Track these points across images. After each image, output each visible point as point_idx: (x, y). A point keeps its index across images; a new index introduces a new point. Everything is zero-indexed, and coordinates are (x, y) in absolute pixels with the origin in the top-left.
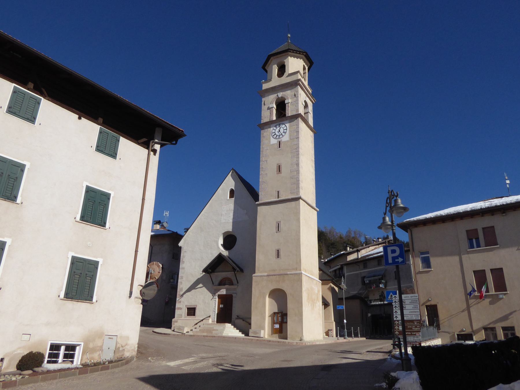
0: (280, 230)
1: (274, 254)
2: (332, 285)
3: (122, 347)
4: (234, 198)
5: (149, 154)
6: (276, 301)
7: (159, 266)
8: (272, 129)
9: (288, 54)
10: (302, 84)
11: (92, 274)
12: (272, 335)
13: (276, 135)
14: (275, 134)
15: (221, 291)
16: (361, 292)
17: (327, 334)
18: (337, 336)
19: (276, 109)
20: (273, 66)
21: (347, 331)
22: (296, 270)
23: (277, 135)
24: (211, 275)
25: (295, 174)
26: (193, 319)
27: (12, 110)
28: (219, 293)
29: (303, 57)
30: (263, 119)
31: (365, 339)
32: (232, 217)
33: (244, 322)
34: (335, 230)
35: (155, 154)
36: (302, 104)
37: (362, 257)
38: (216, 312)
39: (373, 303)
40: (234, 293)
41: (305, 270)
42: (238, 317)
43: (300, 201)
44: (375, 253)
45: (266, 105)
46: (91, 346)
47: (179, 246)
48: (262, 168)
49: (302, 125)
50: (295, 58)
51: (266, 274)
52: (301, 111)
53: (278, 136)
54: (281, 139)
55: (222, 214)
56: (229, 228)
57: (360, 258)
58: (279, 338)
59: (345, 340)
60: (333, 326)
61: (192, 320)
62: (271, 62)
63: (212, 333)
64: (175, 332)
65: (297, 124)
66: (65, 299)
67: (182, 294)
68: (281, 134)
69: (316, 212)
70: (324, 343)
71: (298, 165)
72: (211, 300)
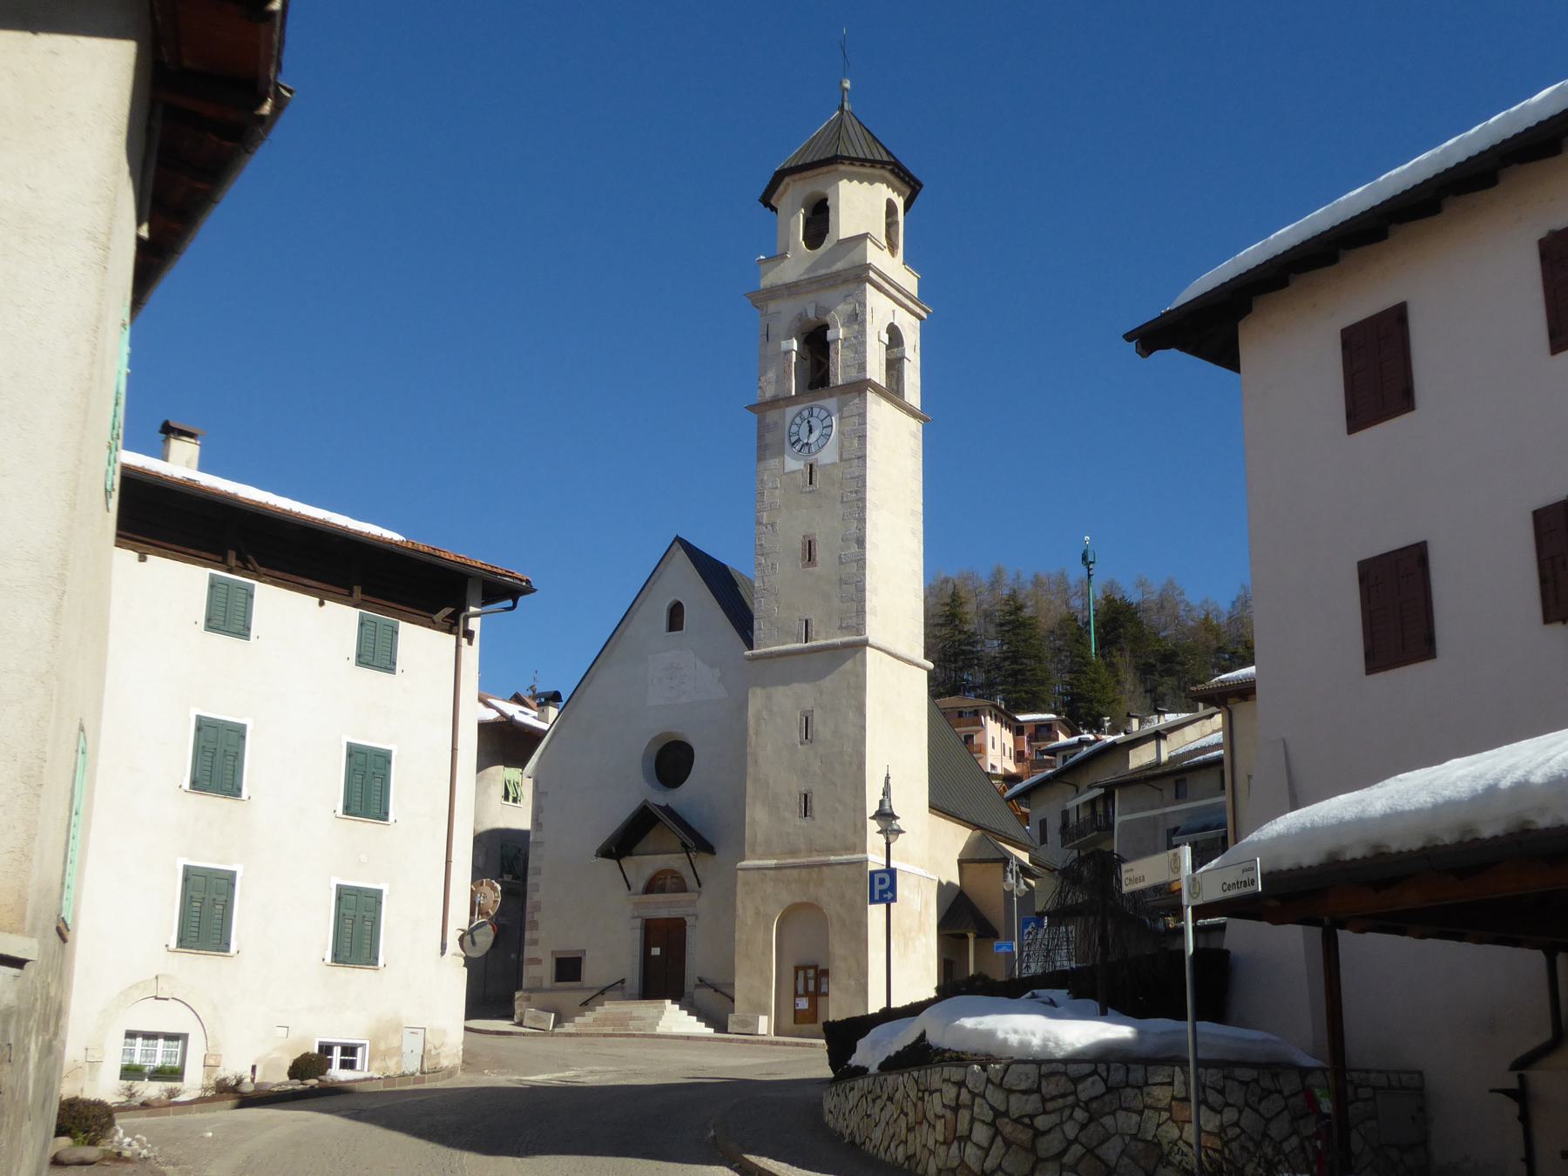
3: (435, 1048)
5: (458, 646)
7: (494, 889)
10: (880, 276)
11: (373, 914)
24: (623, 864)
25: (854, 570)
27: (214, 623)
33: (719, 995)
34: (1181, 593)
35: (470, 643)
40: (688, 915)
46: (382, 1046)
54: (814, 457)
57: (1164, 764)
62: (785, 190)
63: (628, 1025)
65: (861, 411)
66: (334, 964)
71: (861, 542)
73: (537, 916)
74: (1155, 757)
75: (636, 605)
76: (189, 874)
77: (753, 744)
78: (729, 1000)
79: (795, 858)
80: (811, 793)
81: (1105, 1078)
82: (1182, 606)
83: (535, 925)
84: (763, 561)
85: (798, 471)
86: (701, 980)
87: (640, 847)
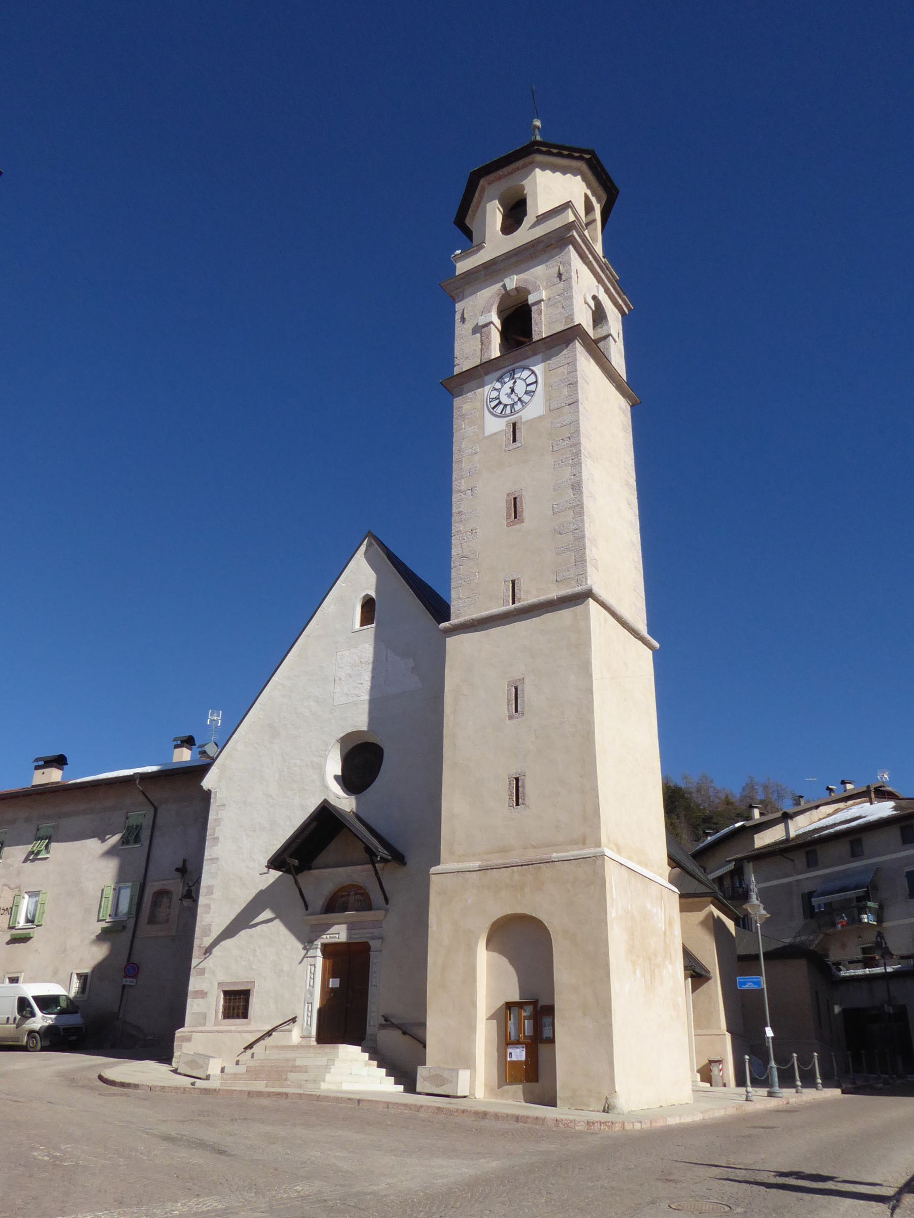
0: (523, 708)
1: (504, 791)
2: (717, 913)
4: (373, 625)
6: (513, 962)
8: (487, 388)
9: (531, 163)
12: (499, 1087)
13: (501, 407)
14: (500, 403)
15: (332, 930)
16: (803, 938)
17: (706, 1074)
18: (740, 1082)
19: (500, 328)
20: (487, 205)
21: (778, 1069)
22: (584, 844)
23: (506, 406)
26: (241, 1028)
28: (326, 938)
29: (583, 166)
30: (458, 365)
31: (838, 1092)
32: (367, 685)
33: (407, 1037)
34: (712, 782)
36: (586, 303)
37: (798, 836)
38: (317, 1005)
39: (843, 973)
40: (373, 938)
41: (617, 845)
42: (388, 1023)
43: (588, 605)
44: (837, 821)
45: (467, 322)
47: (205, 788)
48: (459, 513)
49: (586, 365)
50: (558, 174)
51: (476, 864)
52: (583, 318)
53: (509, 407)
55: (337, 678)
56: (359, 721)
57: (793, 839)
58: (526, 1102)
59: (773, 1103)
60: (726, 1048)
61: (239, 1032)
63: (286, 1079)
65: (570, 360)
67: (207, 945)
68: (519, 399)
69: (651, 652)
70: (698, 1118)
71: (577, 487)
72: (301, 962)
74: (784, 834)
78: (421, 1046)
81: (307, 956)
82: (711, 790)
85: (501, 431)
87: (322, 858)
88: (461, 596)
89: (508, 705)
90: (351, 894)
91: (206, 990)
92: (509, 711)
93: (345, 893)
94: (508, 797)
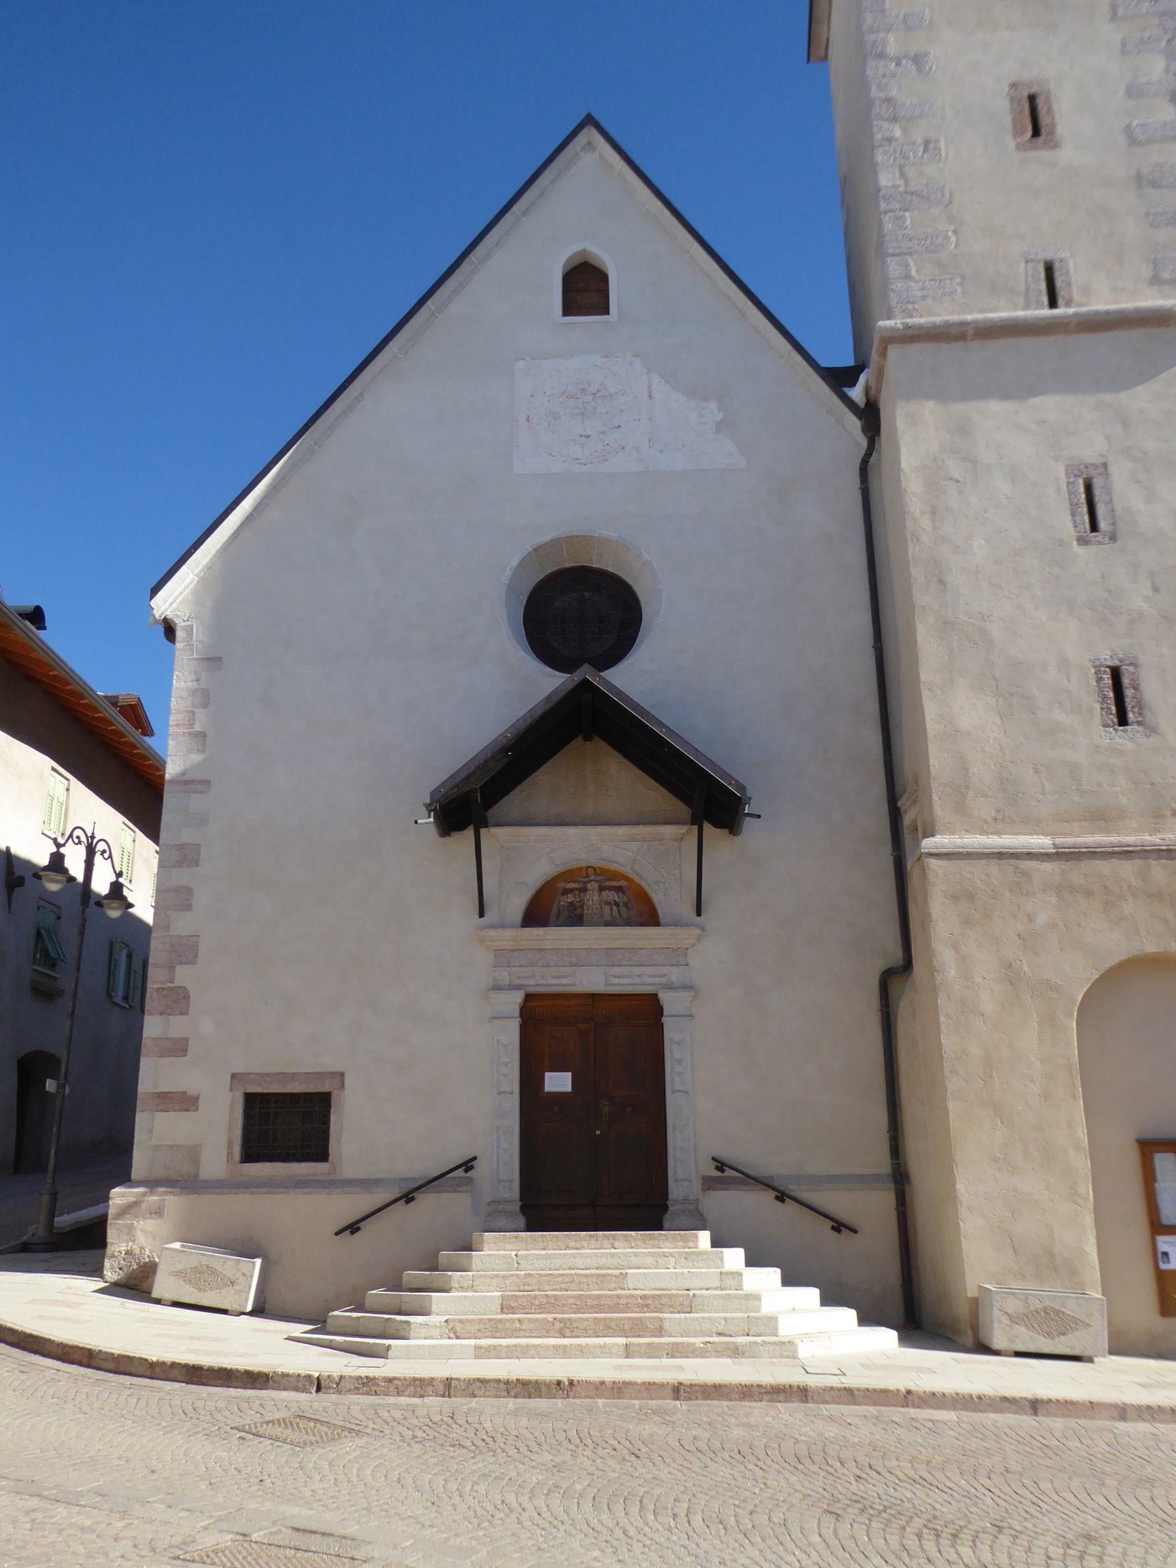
33: (789, 1207)
40: (670, 987)
64: (158, 1301)
73: (184, 976)
75: (480, 250)
76: (609, 314)
77: (925, 538)
79: (1107, 832)
80: (1135, 665)
83: (179, 1000)
84: (898, 133)
86: (721, 1165)
88: (913, 272)
89: (1073, 515)
90: (589, 886)
91: (192, 1092)
92: (1075, 527)
93: (574, 885)
94: (1098, 706)
